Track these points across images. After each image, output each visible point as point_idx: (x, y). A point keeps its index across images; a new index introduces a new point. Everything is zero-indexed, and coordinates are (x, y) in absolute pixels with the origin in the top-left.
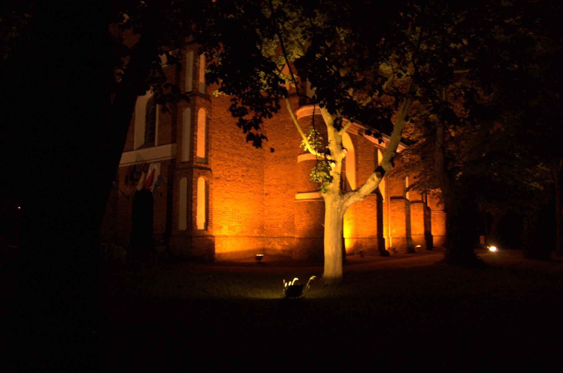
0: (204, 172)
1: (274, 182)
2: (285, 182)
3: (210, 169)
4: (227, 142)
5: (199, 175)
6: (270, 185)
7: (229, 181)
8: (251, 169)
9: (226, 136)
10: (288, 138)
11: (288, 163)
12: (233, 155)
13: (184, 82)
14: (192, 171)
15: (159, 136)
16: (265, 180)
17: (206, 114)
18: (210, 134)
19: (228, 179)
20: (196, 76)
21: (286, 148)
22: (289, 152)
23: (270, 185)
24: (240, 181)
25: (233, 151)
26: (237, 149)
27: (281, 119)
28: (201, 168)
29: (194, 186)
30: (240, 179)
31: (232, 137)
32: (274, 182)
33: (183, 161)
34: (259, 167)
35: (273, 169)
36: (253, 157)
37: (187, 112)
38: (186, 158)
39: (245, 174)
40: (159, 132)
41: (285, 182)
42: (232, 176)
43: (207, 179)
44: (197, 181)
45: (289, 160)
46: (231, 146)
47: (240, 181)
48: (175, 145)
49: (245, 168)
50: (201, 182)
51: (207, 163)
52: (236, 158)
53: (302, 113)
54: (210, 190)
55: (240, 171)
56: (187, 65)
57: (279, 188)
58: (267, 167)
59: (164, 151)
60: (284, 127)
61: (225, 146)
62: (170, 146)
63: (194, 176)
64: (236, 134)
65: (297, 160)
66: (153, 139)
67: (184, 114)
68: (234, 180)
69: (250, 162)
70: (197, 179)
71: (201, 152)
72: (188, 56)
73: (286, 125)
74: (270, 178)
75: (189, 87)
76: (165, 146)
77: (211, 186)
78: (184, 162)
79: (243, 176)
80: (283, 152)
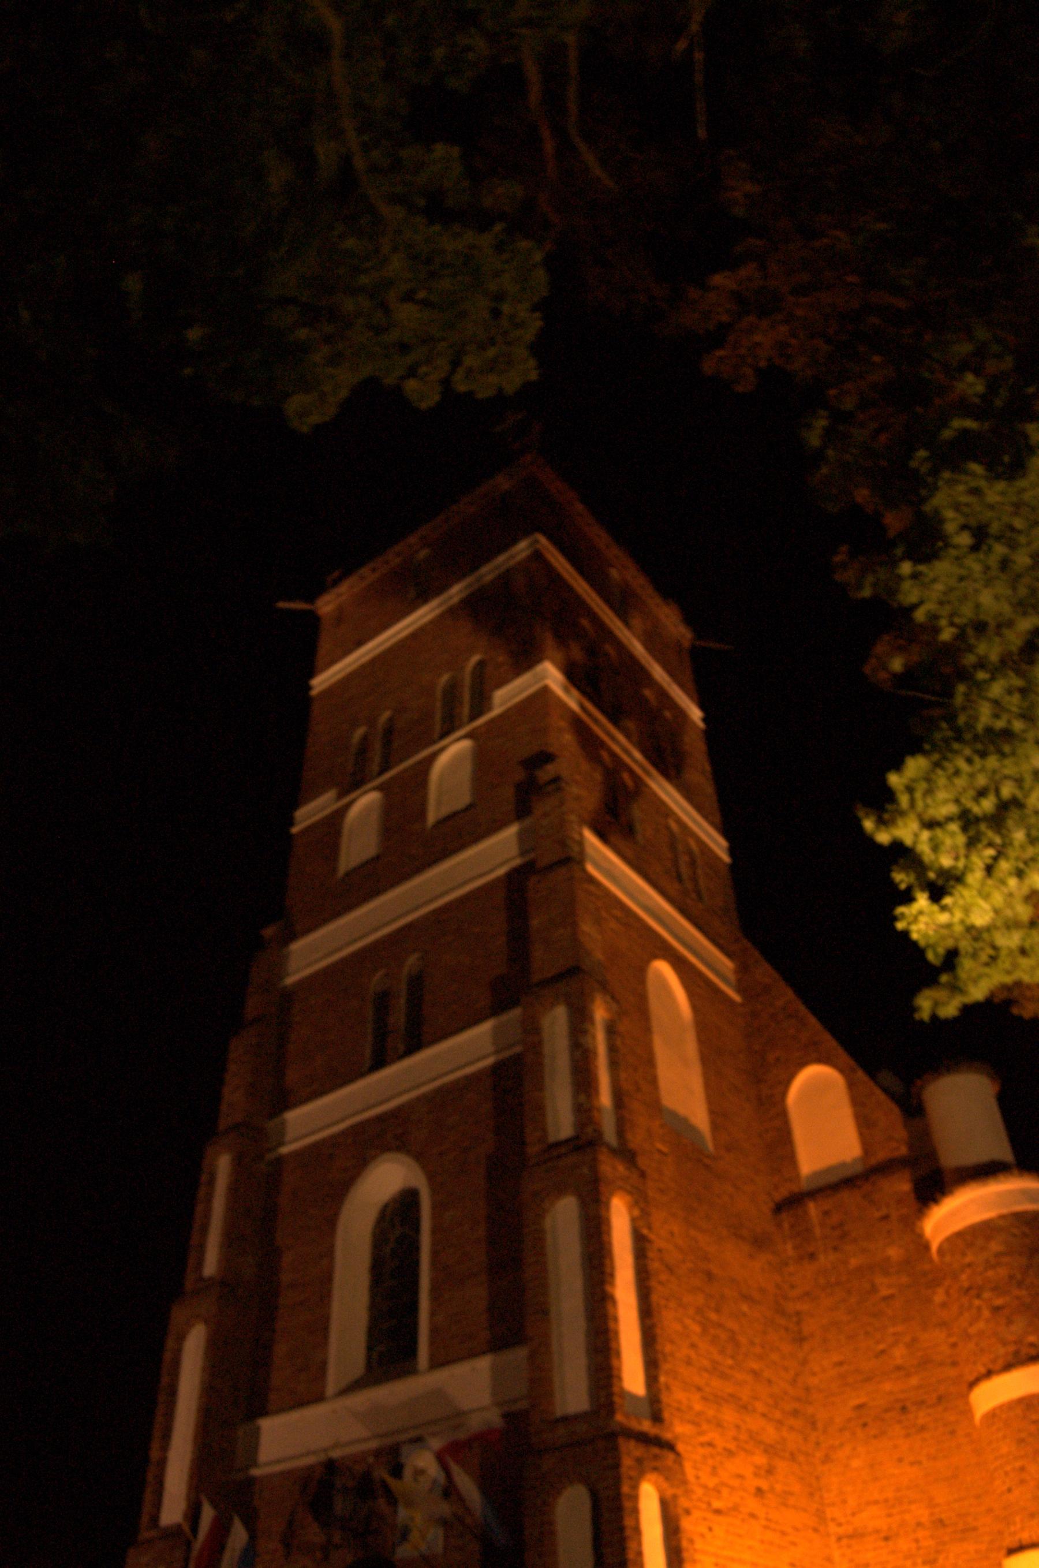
0: (656, 1457)
1: (872, 1518)
2: (922, 1513)
3: (670, 1447)
4: (693, 1346)
5: (641, 1470)
6: (856, 1535)
7: (718, 1512)
8: (782, 1466)
9: (688, 1322)
10: (899, 1328)
11: (923, 1428)
12: (717, 1400)
13: (540, 1108)
14: (616, 1448)
15: (434, 1330)
16: (829, 1512)
17: (633, 1220)
18: (655, 1298)
19: (717, 1504)
20: (583, 1080)
21: (899, 1368)
22: (914, 1381)
23: (856, 1535)
24: (752, 1516)
25: (716, 1383)
26: (724, 1376)
27: (854, 1262)
28: (644, 1439)
29: (628, 1522)
30: (752, 1504)
31: (705, 1330)
32: (872, 1518)
33: (559, 1412)
34: (801, 1458)
35: (855, 1463)
36: (778, 1415)
37: (563, 1215)
38: (572, 1395)
39: (764, 1485)
40: (433, 1314)
41: (922, 1513)
42: (725, 1492)
43: (669, 1492)
44: (635, 1498)
45: (922, 1417)
46: (706, 1363)
47: (752, 1516)
48: (520, 1354)
49: (760, 1459)
50: (648, 1500)
51: (657, 1418)
52: (729, 1415)
53: (953, 1214)
54: (685, 1544)
55: (748, 1472)
56: (547, 1050)
57: (904, 1544)
58: (827, 1459)
59: (471, 1387)
60: (874, 1289)
61: (689, 1362)
62: (484, 1363)
63: (624, 1470)
64: (713, 1316)
65: (967, 1412)
66: (411, 1351)
67: (548, 1223)
68: (735, 1508)
69: (771, 1433)
70: (635, 1487)
71: (632, 1377)
72: (546, 1022)
73: (880, 1280)
74: (852, 1502)
75: (561, 1122)
76: (460, 1370)
77: (687, 1524)
78: (566, 1419)
79: (759, 1492)
80: (888, 1386)
